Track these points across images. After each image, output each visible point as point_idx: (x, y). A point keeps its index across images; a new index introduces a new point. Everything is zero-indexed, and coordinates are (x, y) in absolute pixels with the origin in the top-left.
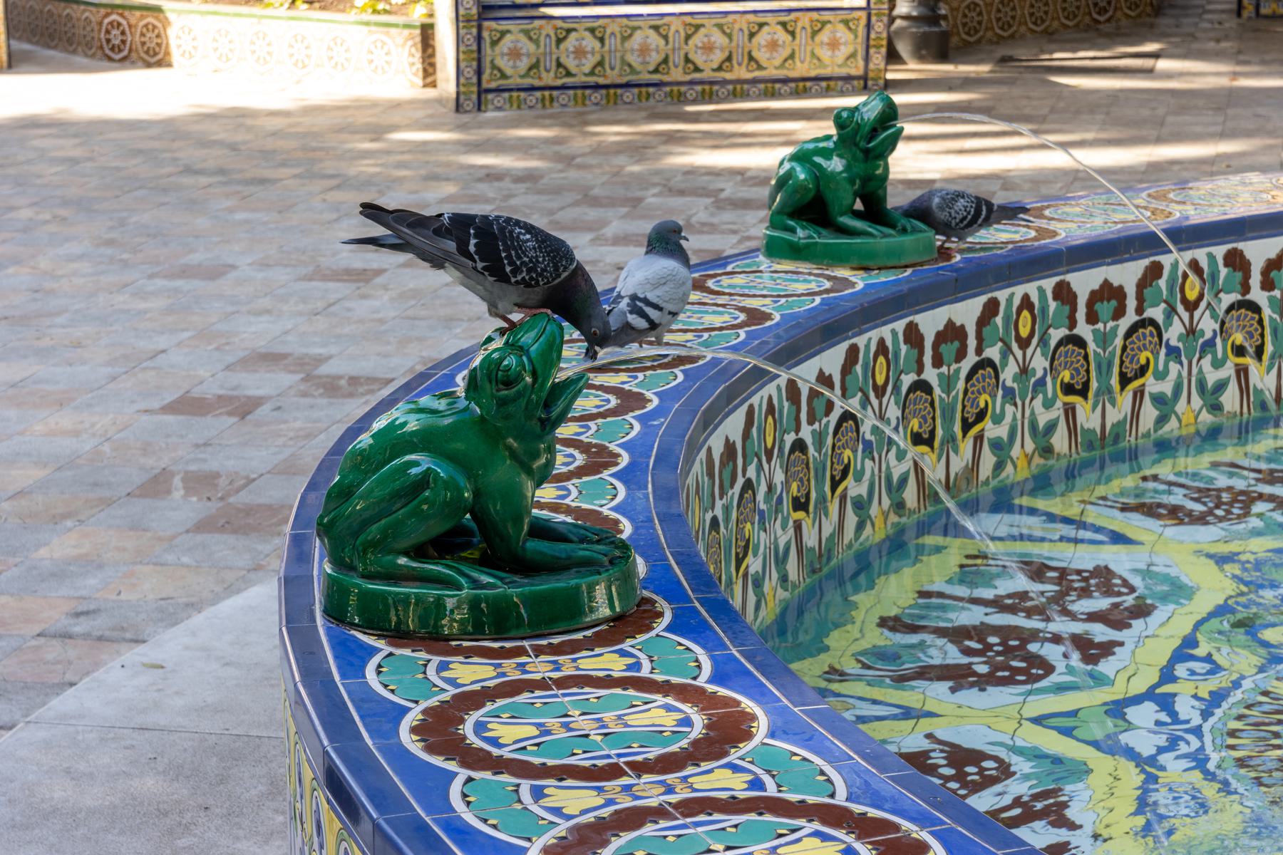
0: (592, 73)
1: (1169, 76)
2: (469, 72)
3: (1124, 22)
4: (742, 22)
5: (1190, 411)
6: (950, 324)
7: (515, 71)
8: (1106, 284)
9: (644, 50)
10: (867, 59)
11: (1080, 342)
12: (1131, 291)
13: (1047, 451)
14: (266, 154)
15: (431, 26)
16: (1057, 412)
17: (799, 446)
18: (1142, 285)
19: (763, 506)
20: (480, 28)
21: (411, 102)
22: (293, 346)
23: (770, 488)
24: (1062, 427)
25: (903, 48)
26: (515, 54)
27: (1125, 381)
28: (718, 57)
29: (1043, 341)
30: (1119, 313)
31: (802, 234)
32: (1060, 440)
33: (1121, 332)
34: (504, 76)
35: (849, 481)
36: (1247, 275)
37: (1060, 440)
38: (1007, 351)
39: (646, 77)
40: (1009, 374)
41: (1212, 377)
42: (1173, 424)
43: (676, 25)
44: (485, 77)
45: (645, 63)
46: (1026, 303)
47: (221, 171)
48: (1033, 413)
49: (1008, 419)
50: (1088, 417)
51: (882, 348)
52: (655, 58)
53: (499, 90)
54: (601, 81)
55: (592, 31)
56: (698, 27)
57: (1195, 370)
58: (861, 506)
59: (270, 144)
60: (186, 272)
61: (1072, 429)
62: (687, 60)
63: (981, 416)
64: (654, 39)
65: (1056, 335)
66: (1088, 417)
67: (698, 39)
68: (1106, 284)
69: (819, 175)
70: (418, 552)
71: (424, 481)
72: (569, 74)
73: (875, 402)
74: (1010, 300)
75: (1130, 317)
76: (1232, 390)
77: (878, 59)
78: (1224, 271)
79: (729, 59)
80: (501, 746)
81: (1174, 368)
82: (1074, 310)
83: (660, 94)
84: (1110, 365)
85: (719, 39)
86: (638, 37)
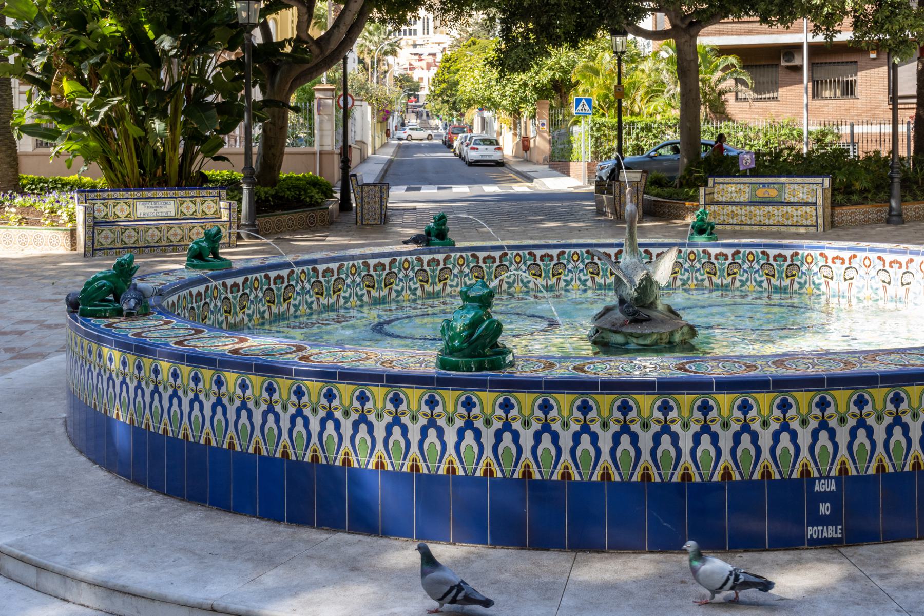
0: (134, 243)
1: (330, 241)
2: (89, 244)
3: (319, 227)
4: (187, 226)
5: (303, 308)
6: (235, 283)
7: (106, 243)
8: (279, 275)
9: (153, 236)
10: (230, 237)
11: (272, 290)
12: (286, 277)
13: (263, 318)
15: (75, 230)
16: (266, 308)
17: (193, 308)
18: (289, 276)
20: (94, 229)
21: (67, 255)
22: (34, 318)
24: (225, 322)
26: (106, 237)
28: (179, 237)
29: (261, 289)
30: (283, 282)
32: (267, 315)
33: (283, 287)
34: (102, 245)
35: (207, 320)
36: (318, 274)
37: (267, 315)
38: (211, 300)
39: (153, 244)
40: (252, 297)
42: (299, 312)
43: (164, 227)
44: (95, 245)
45: (153, 240)
46: (256, 279)
49: (252, 309)
50: (275, 309)
51: (216, 287)
52: (156, 238)
53: (100, 250)
54: (137, 246)
55: (134, 229)
56: (171, 228)
59: (15, 268)
61: (270, 312)
62: (168, 238)
65: (265, 287)
66: (275, 309)
67: (172, 232)
68: (279, 275)
69: (201, 247)
70: (99, 301)
71: (104, 286)
72: (126, 244)
74: (252, 278)
75: (286, 284)
76: (267, 312)
77: (234, 238)
78: (311, 273)
79: (183, 238)
81: (299, 298)
82: (270, 281)
83: (158, 250)
84: (281, 296)
85: (179, 231)
86: (150, 231)
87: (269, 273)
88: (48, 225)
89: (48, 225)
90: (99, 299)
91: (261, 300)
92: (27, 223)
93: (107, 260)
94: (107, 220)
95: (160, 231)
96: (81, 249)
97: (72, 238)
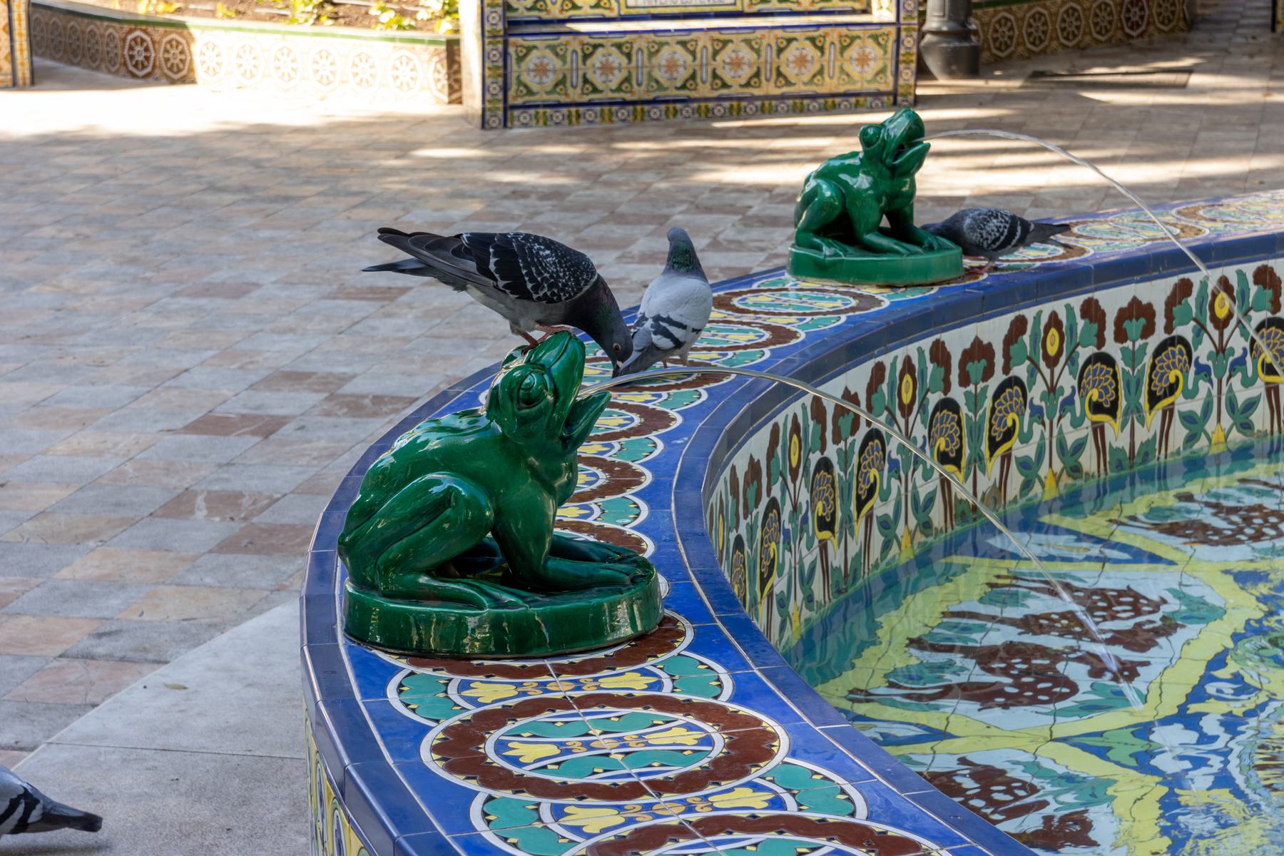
0: (619, 89)
1: (1201, 91)
2: (495, 89)
3: (1157, 36)
4: (770, 38)
6: (977, 342)
7: (541, 87)
8: (1135, 302)
9: (671, 66)
10: (896, 74)
11: (1108, 360)
12: (1160, 309)
13: (1075, 470)
14: (290, 172)
15: (457, 42)
16: (1085, 431)
17: (825, 465)
19: (788, 526)
20: (506, 44)
21: (437, 119)
22: (318, 365)
23: (795, 507)
25: (933, 63)
26: (541, 70)
27: (1154, 399)
28: (746, 72)
29: (1071, 359)
30: (1148, 331)
31: (828, 251)
32: (1088, 460)
33: (1150, 350)
34: (530, 92)
35: (876, 501)
37: (1088, 460)
38: (1034, 369)
39: (673, 93)
40: (1036, 393)
41: (1242, 396)
42: (1203, 442)
43: (704, 40)
44: (511, 93)
45: (672, 79)
46: (1054, 321)
47: (246, 189)
48: (1061, 432)
49: (1036, 438)
50: (1117, 436)
52: (682, 74)
53: (525, 107)
54: (628, 97)
56: (725, 43)
57: (1225, 389)
58: (887, 525)
59: (294, 160)
60: (209, 291)
61: (1101, 448)
62: (715, 76)
63: (1008, 435)
64: (682, 55)
65: (1085, 353)
66: (1117, 436)
67: (725, 55)
68: (1135, 302)
69: (845, 193)
71: (445, 501)
72: (595, 90)
73: (901, 421)
74: (1037, 318)
75: (1159, 336)
76: (1090, 449)
77: (908, 75)
78: (1254, 289)
79: (757, 75)
80: (521, 765)
81: (1203, 386)
83: (687, 110)
84: (1139, 383)
85: (746, 54)
86: (665, 53)
87: (1099, 295)
88: (388, 26)
89: (388, 26)
90: (426, 562)
91: (1069, 401)
92: (335, 17)
93: (544, 140)
94: (544, 16)
95: (693, 53)
96: (473, 99)
97: (450, 65)
